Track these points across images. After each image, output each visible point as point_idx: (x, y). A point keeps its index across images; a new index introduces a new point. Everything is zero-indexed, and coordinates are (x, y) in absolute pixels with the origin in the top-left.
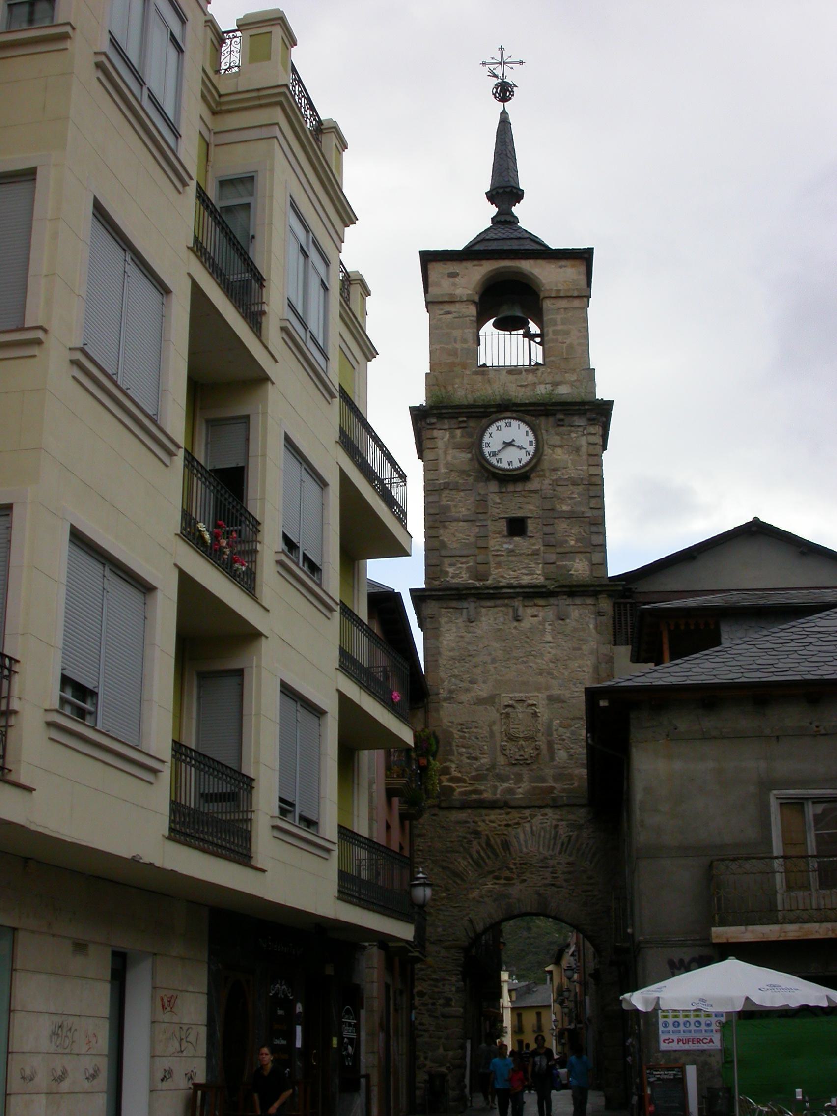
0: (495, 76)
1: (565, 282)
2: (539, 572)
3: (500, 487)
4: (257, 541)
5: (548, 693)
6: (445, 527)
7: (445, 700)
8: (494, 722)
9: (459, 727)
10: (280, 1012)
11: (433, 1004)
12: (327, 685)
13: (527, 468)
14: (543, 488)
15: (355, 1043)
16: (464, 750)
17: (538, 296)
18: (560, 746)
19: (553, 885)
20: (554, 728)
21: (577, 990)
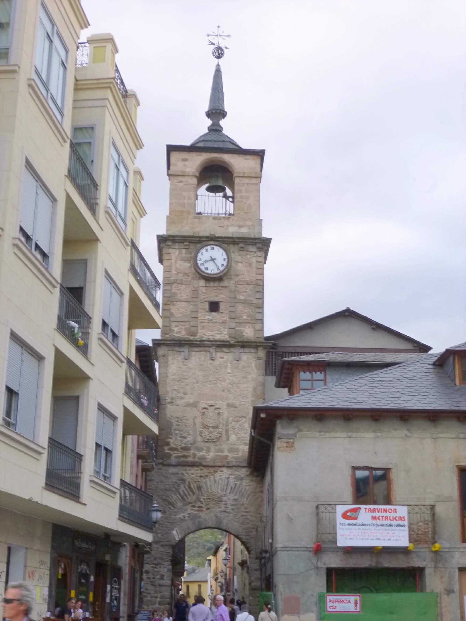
0: (213, 44)
2: (225, 333)
3: (206, 284)
4: (89, 328)
5: (227, 402)
6: (173, 305)
7: (170, 403)
8: (196, 417)
9: (176, 419)
10: (83, 581)
11: (154, 578)
12: (118, 402)
13: (222, 274)
14: (230, 285)
15: (118, 599)
16: (178, 432)
17: (232, 175)
18: (232, 432)
19: (225, 512)
20: (230, 422)
21: (228, 573)
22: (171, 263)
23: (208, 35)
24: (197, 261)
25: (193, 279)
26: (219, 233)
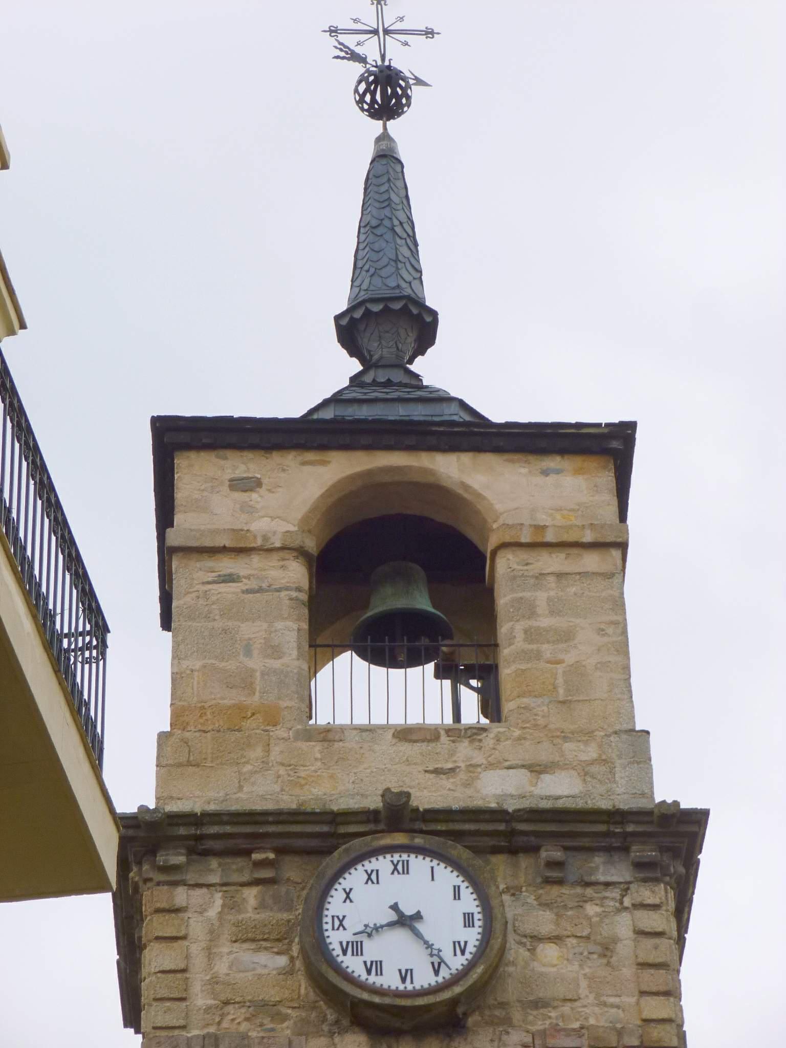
0: (362, 60)
1: (559, 510)
13: (457, 989)
22: (187, 957)
23: (333, 31)
24: (321, 930)
25: (305, 1030)
26: (428, 795)
